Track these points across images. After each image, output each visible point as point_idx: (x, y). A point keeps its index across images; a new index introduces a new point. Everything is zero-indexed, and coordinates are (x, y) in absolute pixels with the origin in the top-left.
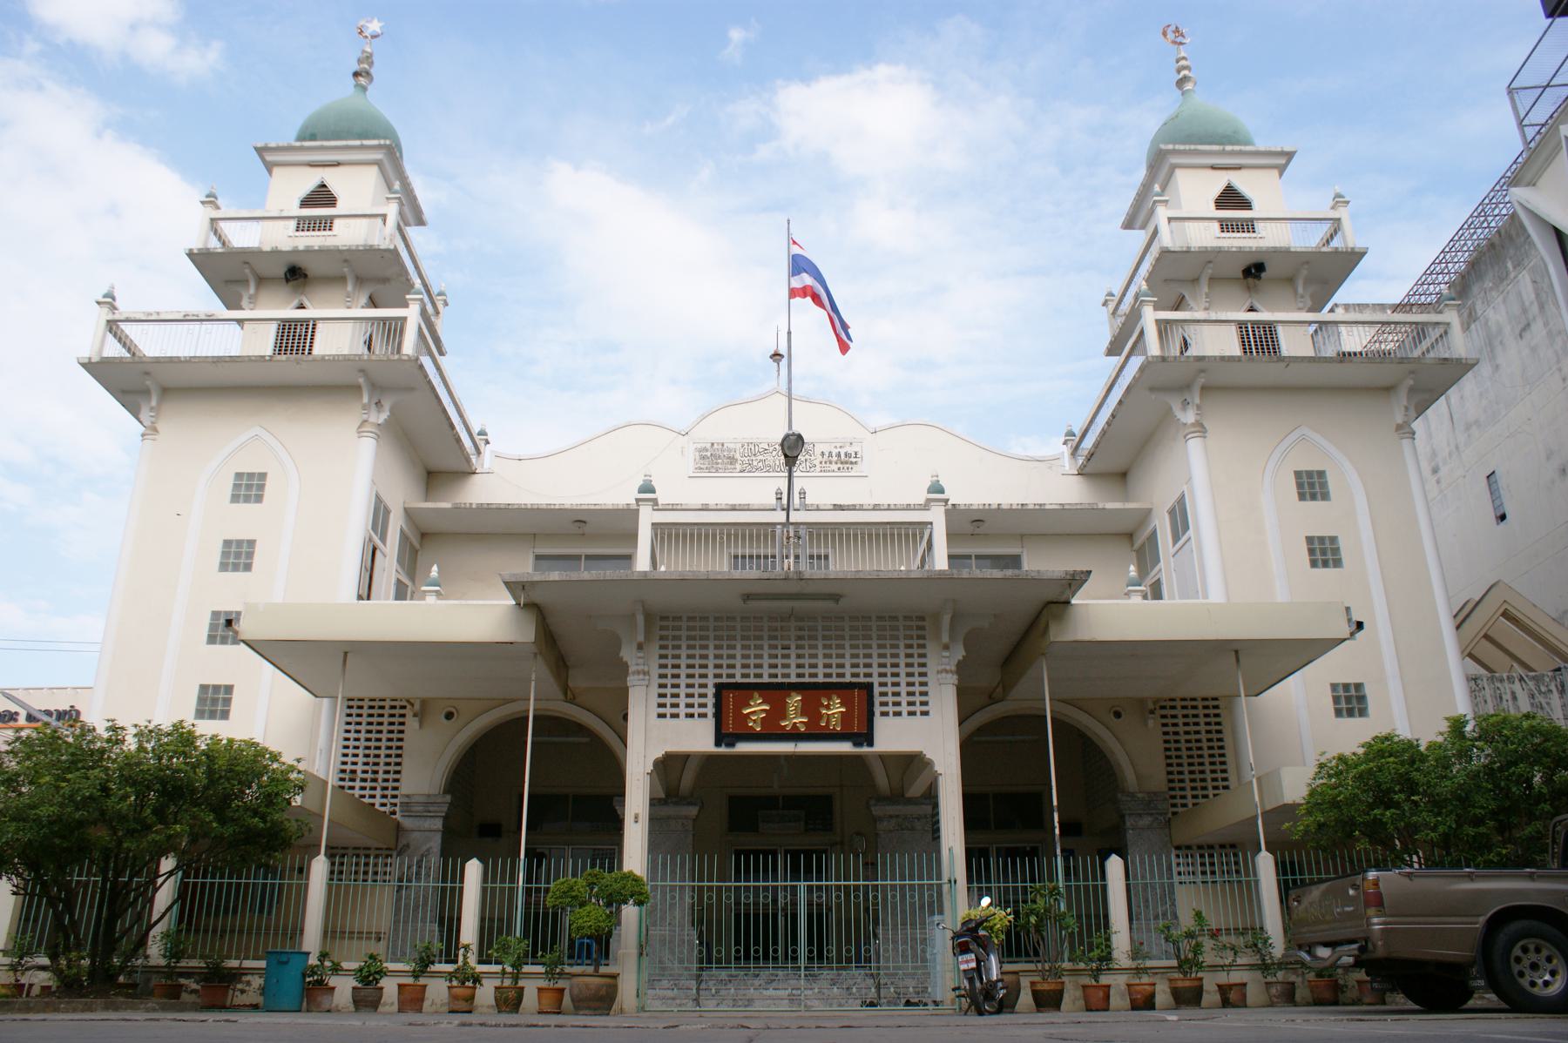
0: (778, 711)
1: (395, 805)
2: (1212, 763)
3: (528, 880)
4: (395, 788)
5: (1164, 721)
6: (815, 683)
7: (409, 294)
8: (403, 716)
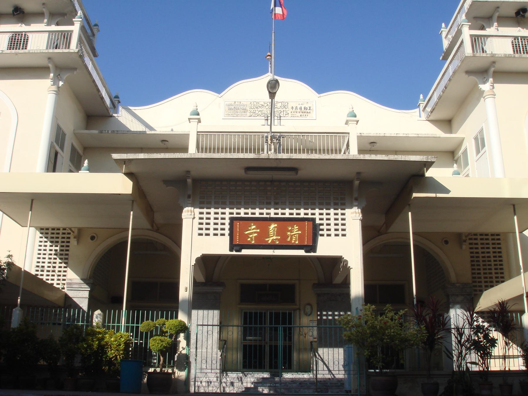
0: (265, 233)
1: (64, 284)
2: (496, 269)
3: (128, 322)
4: (64, 276)
5: (471, 246)
6: (284, 218)
7: (75, 18)
8: (69, 238)
